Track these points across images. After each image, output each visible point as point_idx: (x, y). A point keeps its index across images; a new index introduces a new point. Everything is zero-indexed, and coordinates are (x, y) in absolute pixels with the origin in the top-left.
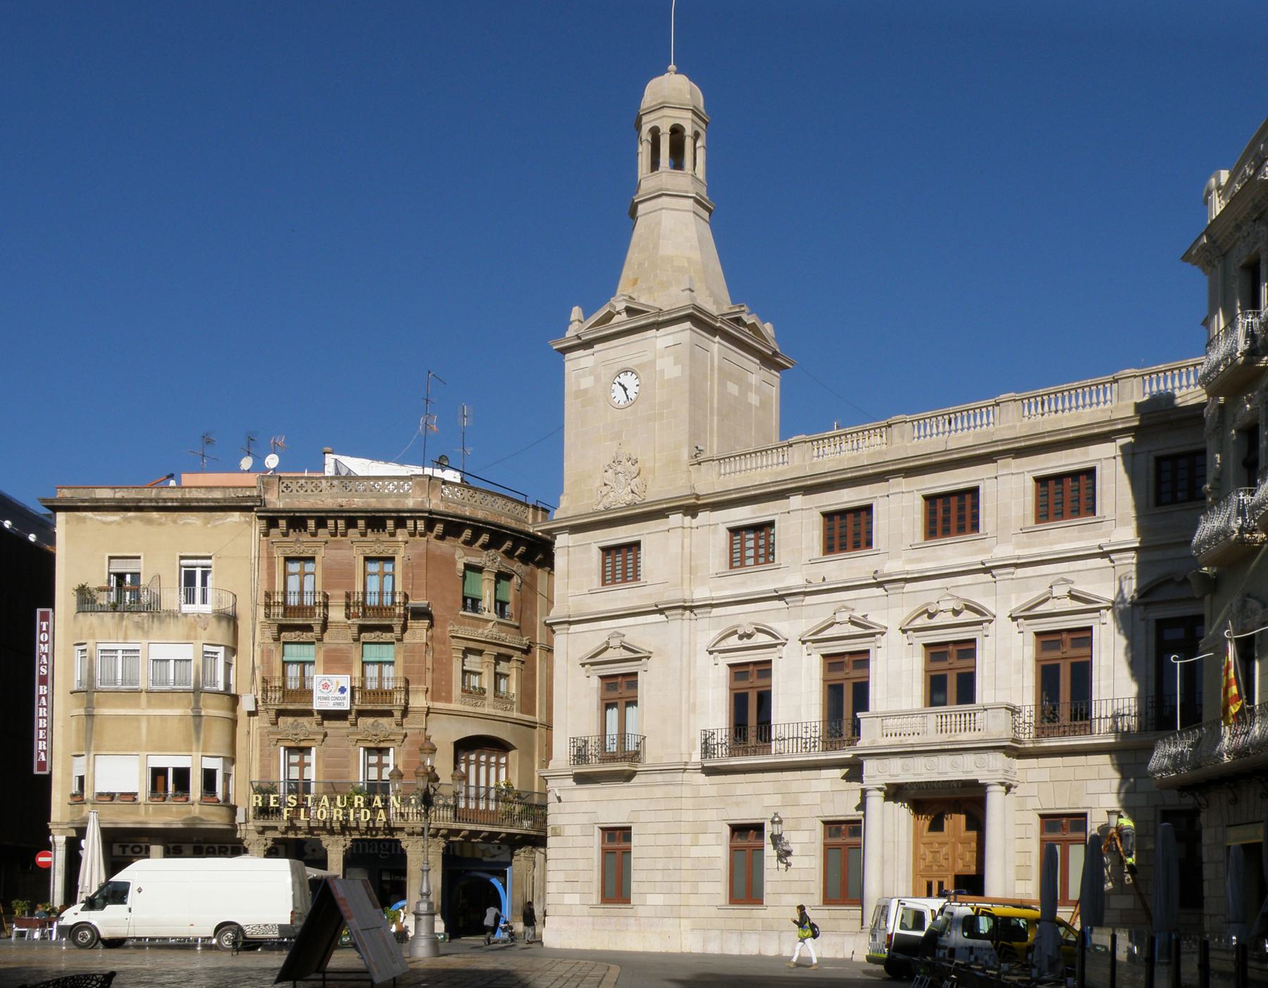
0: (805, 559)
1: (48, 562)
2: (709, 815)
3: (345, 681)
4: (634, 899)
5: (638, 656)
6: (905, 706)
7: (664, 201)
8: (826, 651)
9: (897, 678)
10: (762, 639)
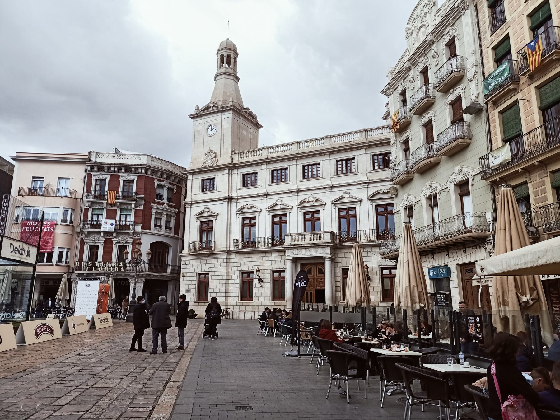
1: (10, 179)
2: (235, 269)
3: (113, 221)
6: (300, 232)
8: (273, 214)
9: (295, 223)
10: (254, 209)
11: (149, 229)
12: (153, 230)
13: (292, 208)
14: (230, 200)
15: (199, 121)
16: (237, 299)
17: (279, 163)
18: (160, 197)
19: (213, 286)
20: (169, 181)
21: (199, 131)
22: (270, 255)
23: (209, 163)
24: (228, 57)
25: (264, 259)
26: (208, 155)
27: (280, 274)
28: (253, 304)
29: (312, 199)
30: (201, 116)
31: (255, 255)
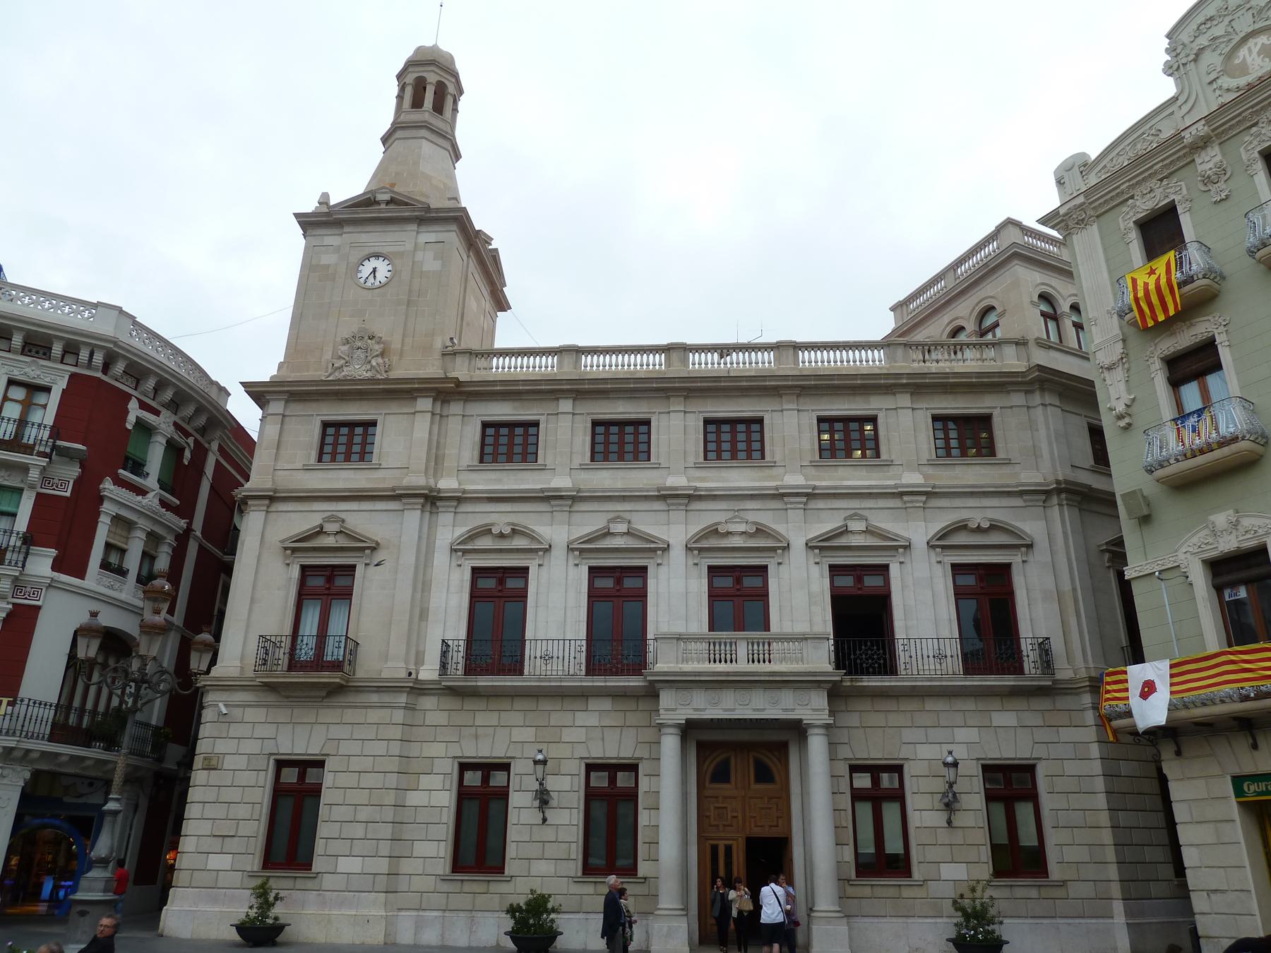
0: (576, 464)
2: (437, 750)
4: (318, 865)
7: (424, 133)
8: (594, 563)
11: (81, 574)
12: (94, 578)
13: (548, 550)
14: (431, 500)
15: (331, 239)
16: (444, 866)
17: (620, 403)
18: (138, 467)
19: (338, 813)
20: (174, 418)
22: (578, 704)
23: (358, 370)
24: (429, 90)
25: (556, 719)
28: (504, 888)
29: (742, 528)
31: (520, 704)
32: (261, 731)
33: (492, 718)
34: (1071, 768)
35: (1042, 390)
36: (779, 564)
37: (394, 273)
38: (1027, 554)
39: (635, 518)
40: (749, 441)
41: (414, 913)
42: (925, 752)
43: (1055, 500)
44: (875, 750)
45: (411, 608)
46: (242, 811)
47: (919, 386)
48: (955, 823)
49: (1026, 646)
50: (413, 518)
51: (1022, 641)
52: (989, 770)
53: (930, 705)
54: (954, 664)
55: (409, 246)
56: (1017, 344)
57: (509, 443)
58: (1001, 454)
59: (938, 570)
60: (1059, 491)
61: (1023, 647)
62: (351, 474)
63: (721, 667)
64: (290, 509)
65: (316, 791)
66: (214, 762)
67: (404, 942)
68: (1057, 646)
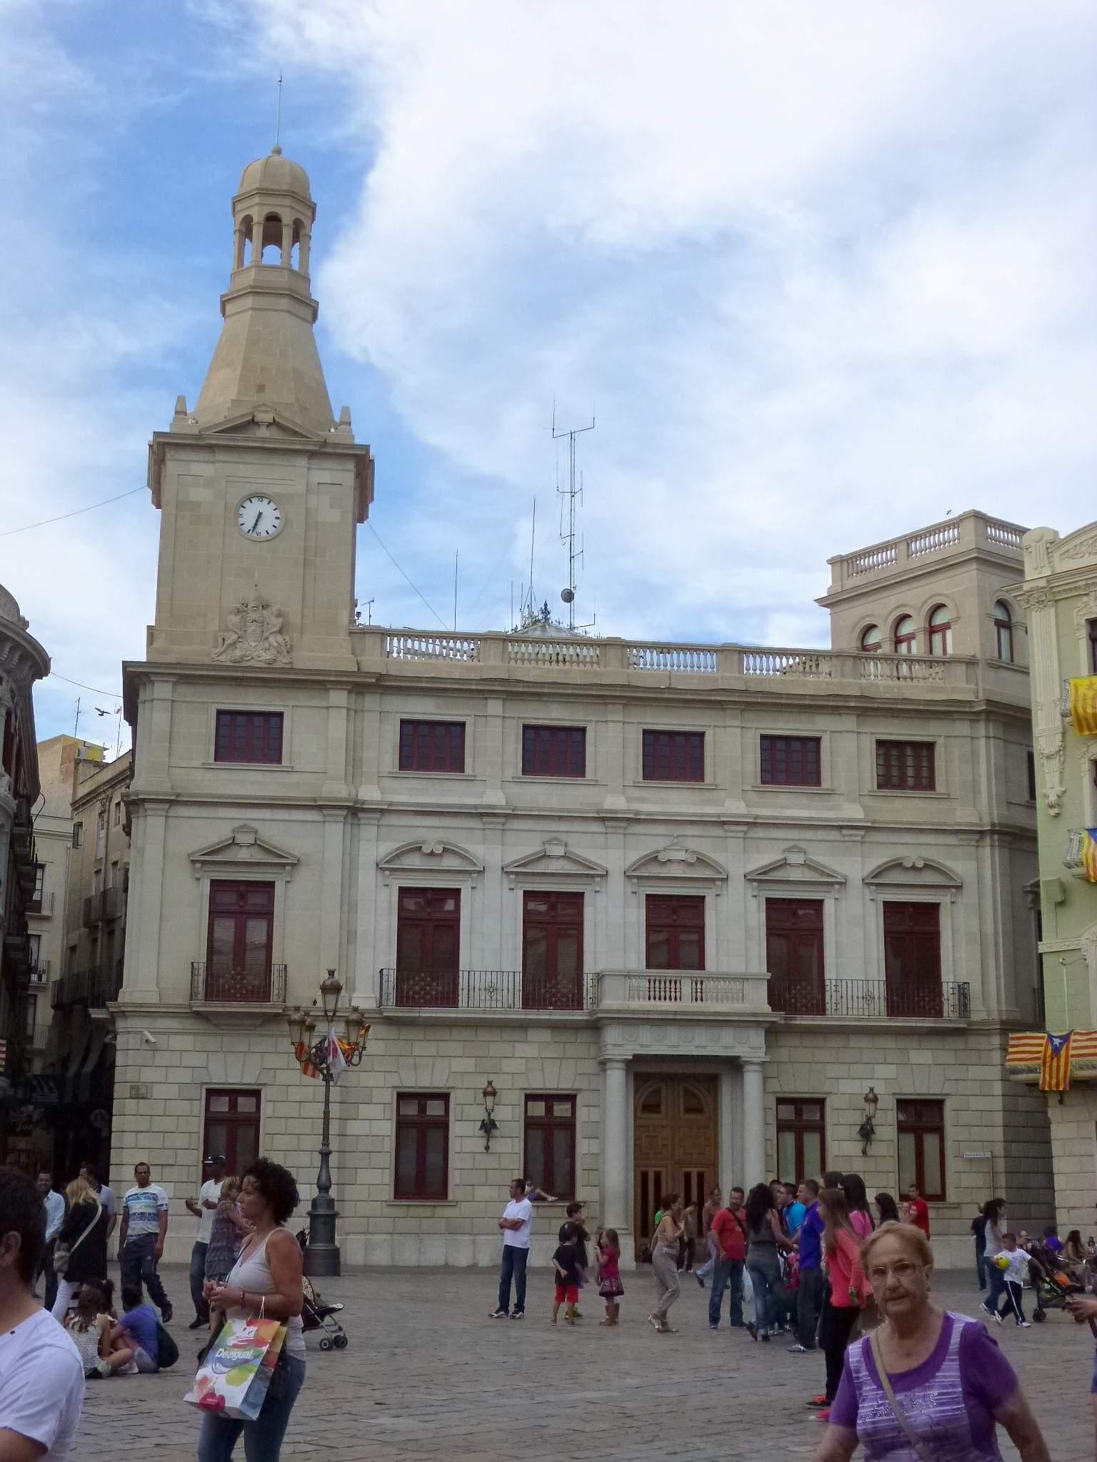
5: (289, 864)
8: (530, 887)
10: (451, 862)
14: (355, 811)
16: (388, 1192)
17: (554, 706)
21: (197, 505)
22: (517, 1035)
25: (495, 1049)
26: (253, 615)
27: (549, 1110)
28: (450, 1212)
29: (682, 856)
30: (211, 448)
31: (459, 1034)
32: (189, 1060)
33: (431, 1049)
34: (977, 1103)
35: (987, 720)
36: (288, 882)
37: (286, 522)
38: (291, 874)
39: (570, 839)
40: (917, 768)
41: (363, 1237)
42: (847, 1087)
43: (988, 841)
44: (800, 1085)
45: (336, 933)
46: (180, 1140)
47: (866, 708)
48: (492, 1149)
49: (948, 989)
50: (335, 830)
51: (944, 985)
52: (903, 1104)
53: (855, 1042)
54: (880, 1005)
55: (300, 488)
56: (967, 663)
57: (433, 747)
58: (940, 787)
59: (753, 904)
60: (993, 832)
61: (945, 992)
62: (258, 776)
63: (666, 1005)
64: (193, 814)
65: (569, 1125)
66: (143, 1091)
67: (353, 1263)
68: (975, 990)
